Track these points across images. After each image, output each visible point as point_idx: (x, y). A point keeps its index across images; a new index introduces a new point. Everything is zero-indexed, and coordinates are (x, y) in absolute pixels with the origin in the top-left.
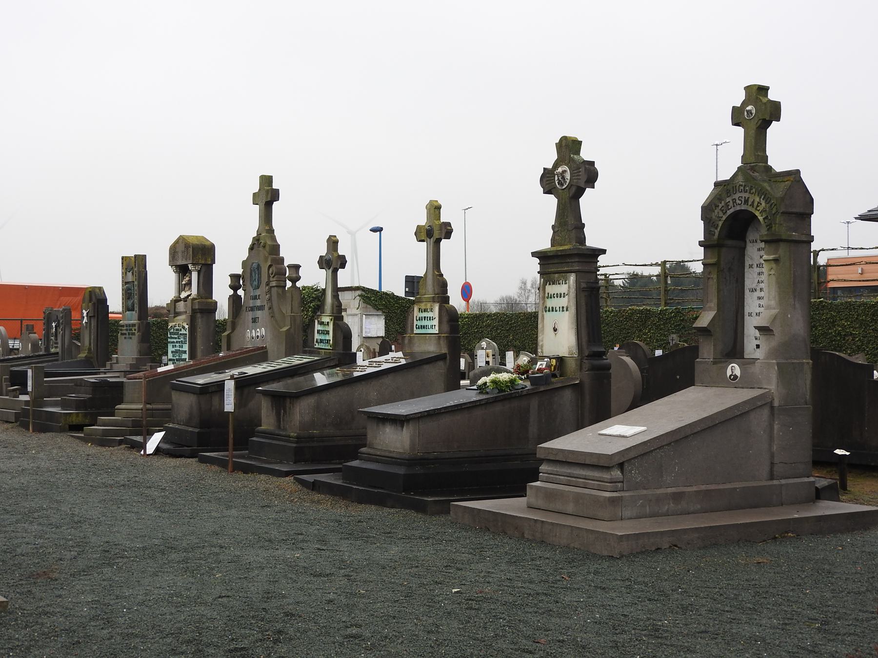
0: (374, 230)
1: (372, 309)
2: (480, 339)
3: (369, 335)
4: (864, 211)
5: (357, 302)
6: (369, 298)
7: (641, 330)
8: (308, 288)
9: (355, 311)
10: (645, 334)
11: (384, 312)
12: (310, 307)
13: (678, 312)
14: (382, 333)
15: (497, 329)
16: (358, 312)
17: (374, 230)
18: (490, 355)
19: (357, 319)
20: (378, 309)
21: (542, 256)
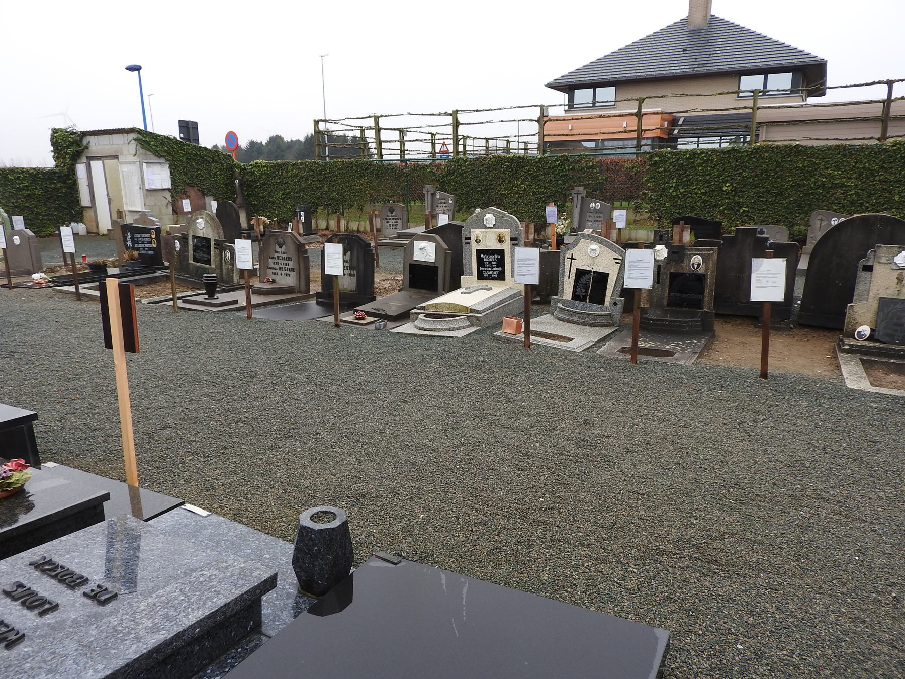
0: (131, 69)
1: (153, 156)
2: (485, 206)
3: (153, 187)
4: (551, 80)
5: (133, 146)
6: (148, 143)
7: (509, 182)
8: (62, 130)
9: (131, 159)
10: (518, 186)
11: (167, 160)
12: (67, 154)
13: (565, 159)
14: (168, 184)
15: (307, 179)
16: (135, 159)
17: (131, 69)
18: (507, 239)
19: (134, 168)
20: (160, 157)
21: (189, 128)
